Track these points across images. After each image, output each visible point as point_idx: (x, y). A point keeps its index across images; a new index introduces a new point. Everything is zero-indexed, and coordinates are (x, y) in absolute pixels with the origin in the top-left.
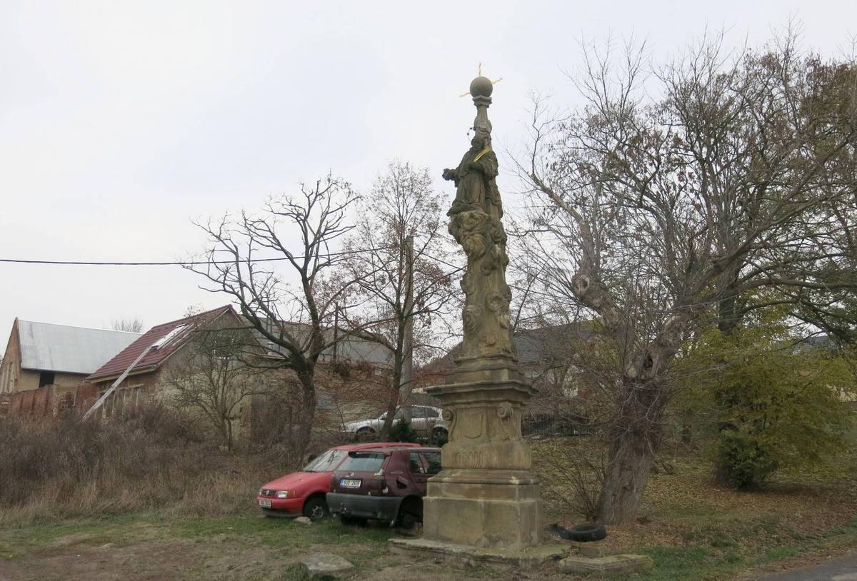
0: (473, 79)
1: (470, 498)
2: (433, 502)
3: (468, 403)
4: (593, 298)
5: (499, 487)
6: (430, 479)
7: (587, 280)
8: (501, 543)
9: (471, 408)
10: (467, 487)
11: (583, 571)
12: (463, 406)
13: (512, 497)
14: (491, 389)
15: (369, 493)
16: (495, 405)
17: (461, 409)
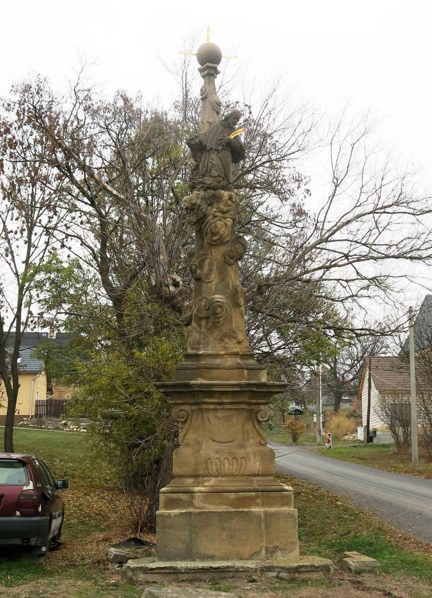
0: (198, 47)
1: (238, 508)
2: (175, 516)
3: (220, 404)
4: (184, 300)
5: (272, 494)
6: (163, 489)
7: (179, 279)
8: (279, 553)
9: (223, 409)
10: (233, 496)
11: (367, 568)
12: (212, 407)
13: (287, 504)
14: (259, 390)
15: (18, 513)
16: (253, 407)
17: (209, 410)
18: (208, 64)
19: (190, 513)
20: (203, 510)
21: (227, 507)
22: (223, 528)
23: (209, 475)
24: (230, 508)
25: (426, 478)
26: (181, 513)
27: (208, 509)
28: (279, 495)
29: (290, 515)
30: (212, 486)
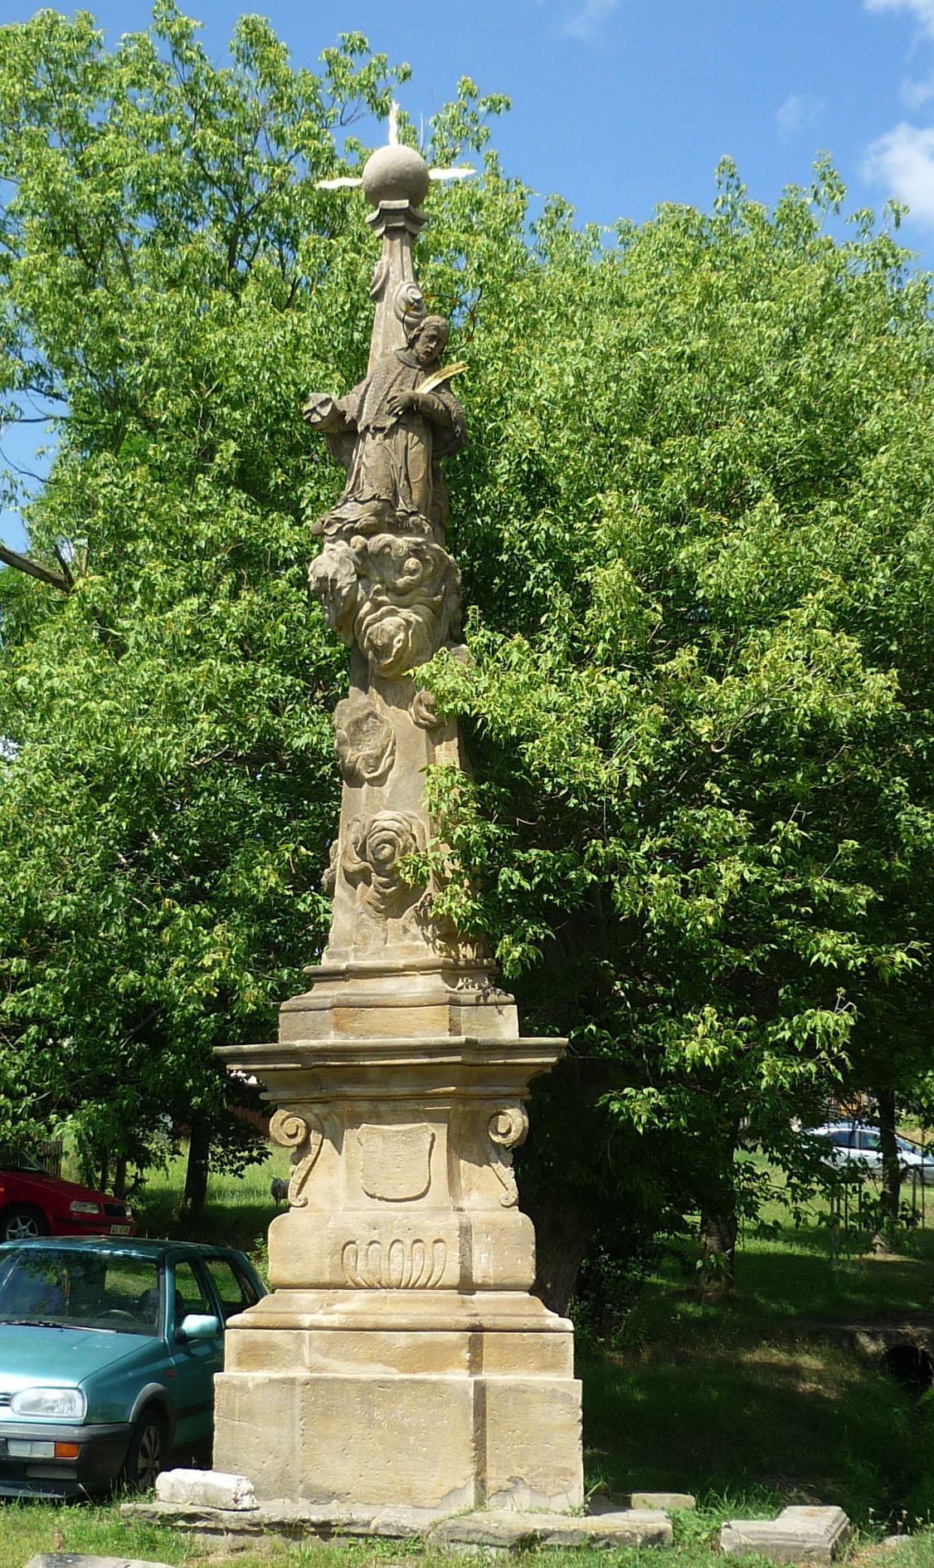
2: (257, 1386)
10: (403, 1339)
18: (384, 203)
19: (292, 1381)
20: (323, 1375)
21: (387, 1369)
22: (371, 1423)
23: (350, 1283)
24: (394, 1370)
25: (259, 1258)
26: (271, 1381)
27: (335, 1371)
28: (531, 1341)
29: (553, 1395)
30: (353, 1313)
